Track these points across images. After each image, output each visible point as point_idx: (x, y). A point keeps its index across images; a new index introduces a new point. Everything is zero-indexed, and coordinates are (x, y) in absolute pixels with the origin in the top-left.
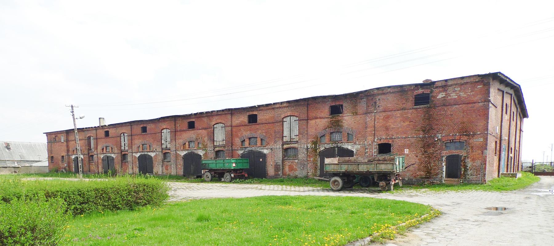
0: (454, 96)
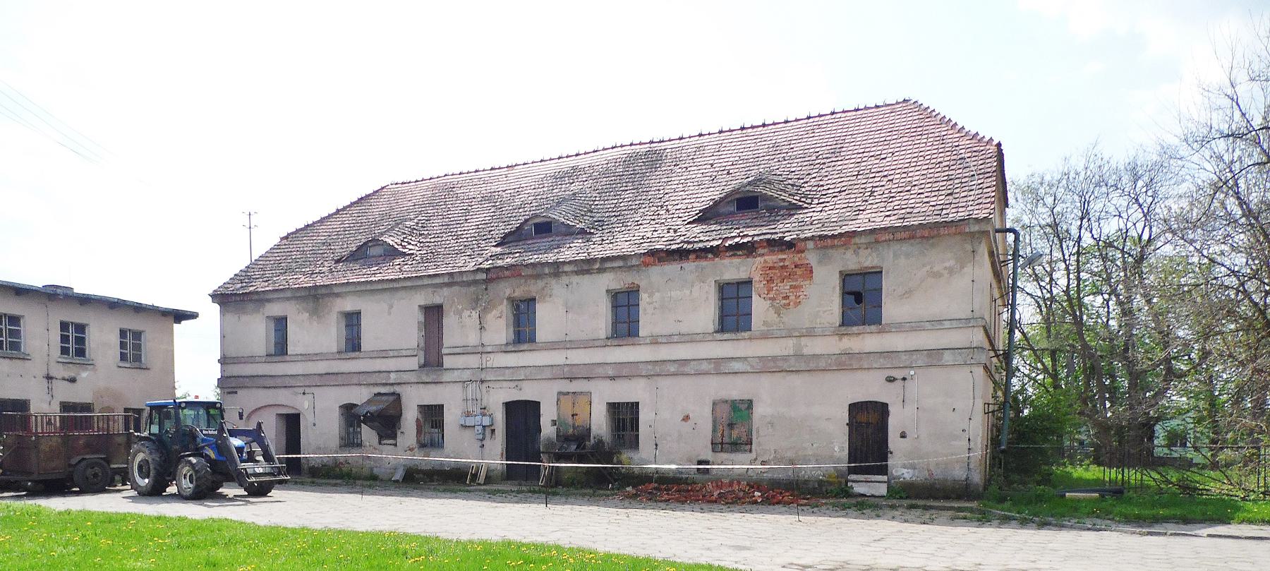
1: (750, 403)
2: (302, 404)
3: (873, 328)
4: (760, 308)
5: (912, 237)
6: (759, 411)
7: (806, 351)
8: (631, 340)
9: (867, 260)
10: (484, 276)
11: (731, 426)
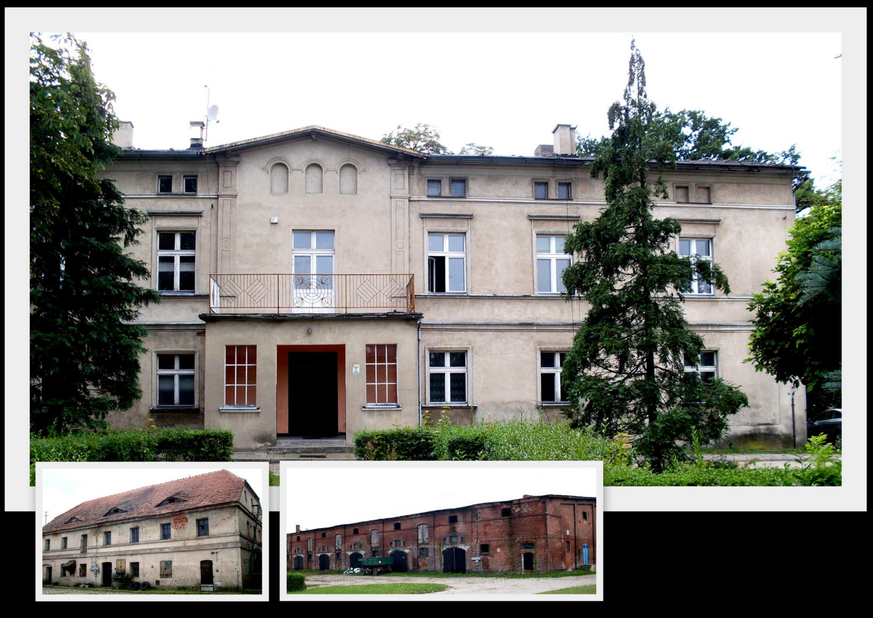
0: (525, 510)
1: (171, 562)
2: (52, 564)
3: (207, 537)
4: (173, 531)
5: (216, 508)
6: (174, 564)
7: (187, 545)
8: (137, 543)
9: (204, 515)
10: (97, 526)
11: (165, 569)
